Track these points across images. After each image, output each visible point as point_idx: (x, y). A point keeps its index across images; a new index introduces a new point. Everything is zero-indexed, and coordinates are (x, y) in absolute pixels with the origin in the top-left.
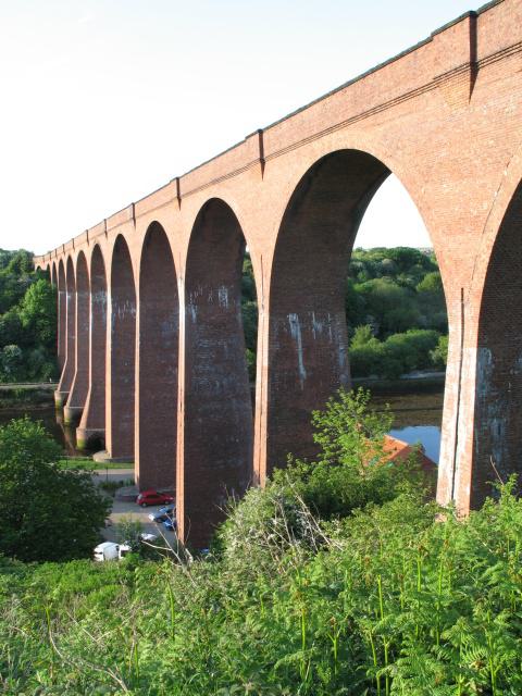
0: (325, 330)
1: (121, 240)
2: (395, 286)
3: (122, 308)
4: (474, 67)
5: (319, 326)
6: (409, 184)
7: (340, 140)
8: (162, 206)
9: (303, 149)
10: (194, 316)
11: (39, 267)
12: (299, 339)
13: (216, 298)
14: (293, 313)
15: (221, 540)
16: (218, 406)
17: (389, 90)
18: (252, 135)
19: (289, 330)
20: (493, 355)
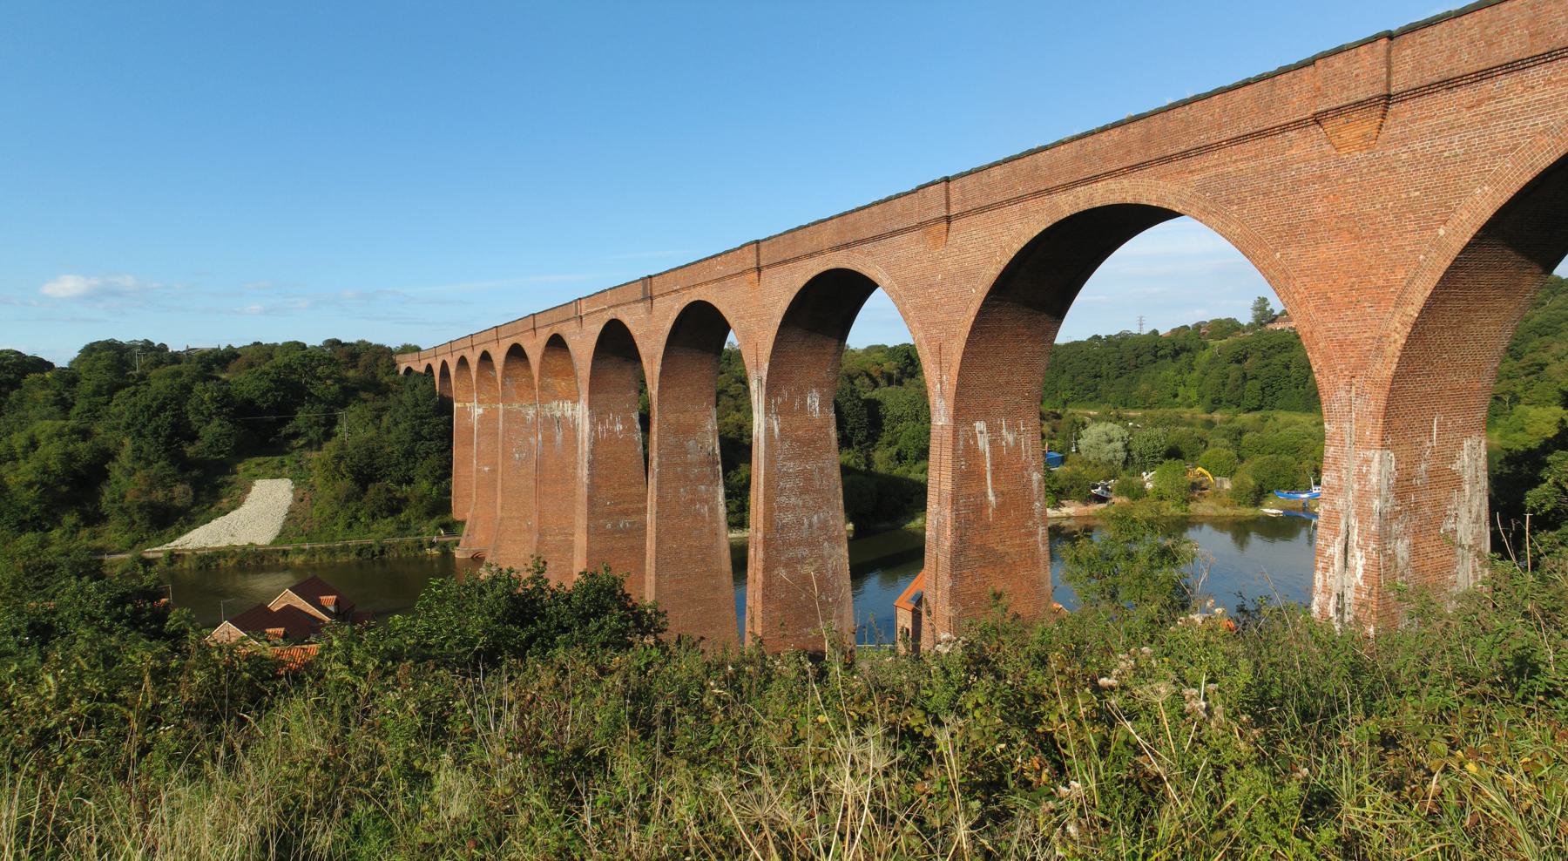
0: (1017, 444)
3: (603, 424)
5: (1010, 438)
6: (890, 292)
9: (1046, 201)
10: (777, 430)
13: (803, 406)
15: (62, 463)
19: (976, 442)
20: (1398, 460)
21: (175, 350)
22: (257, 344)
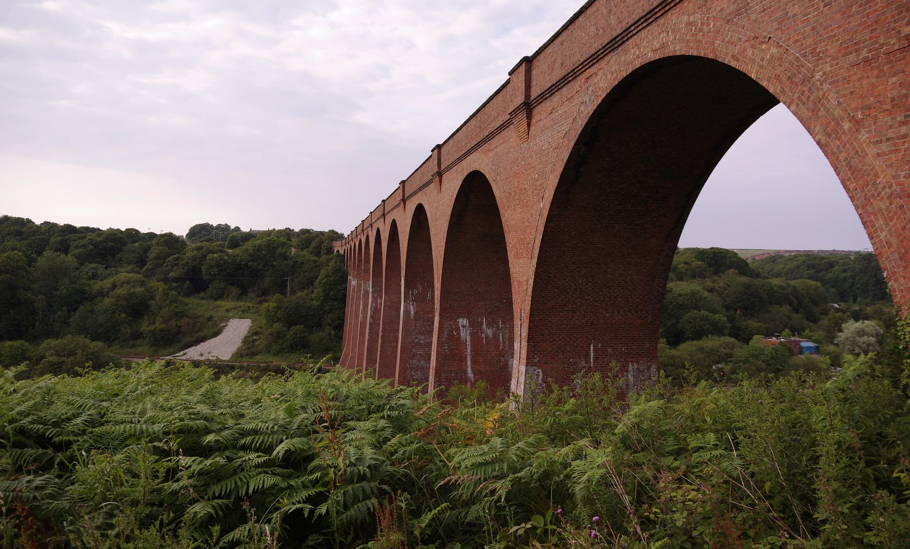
0: (496, 337)
2: (111, 299)
4: (440, 174)
5: (490, 332)
10: (412, 312)
11: (338, 251)
14: (463, 317)
19: (459, 334)
21: (187, 232)
22: (171, 234)
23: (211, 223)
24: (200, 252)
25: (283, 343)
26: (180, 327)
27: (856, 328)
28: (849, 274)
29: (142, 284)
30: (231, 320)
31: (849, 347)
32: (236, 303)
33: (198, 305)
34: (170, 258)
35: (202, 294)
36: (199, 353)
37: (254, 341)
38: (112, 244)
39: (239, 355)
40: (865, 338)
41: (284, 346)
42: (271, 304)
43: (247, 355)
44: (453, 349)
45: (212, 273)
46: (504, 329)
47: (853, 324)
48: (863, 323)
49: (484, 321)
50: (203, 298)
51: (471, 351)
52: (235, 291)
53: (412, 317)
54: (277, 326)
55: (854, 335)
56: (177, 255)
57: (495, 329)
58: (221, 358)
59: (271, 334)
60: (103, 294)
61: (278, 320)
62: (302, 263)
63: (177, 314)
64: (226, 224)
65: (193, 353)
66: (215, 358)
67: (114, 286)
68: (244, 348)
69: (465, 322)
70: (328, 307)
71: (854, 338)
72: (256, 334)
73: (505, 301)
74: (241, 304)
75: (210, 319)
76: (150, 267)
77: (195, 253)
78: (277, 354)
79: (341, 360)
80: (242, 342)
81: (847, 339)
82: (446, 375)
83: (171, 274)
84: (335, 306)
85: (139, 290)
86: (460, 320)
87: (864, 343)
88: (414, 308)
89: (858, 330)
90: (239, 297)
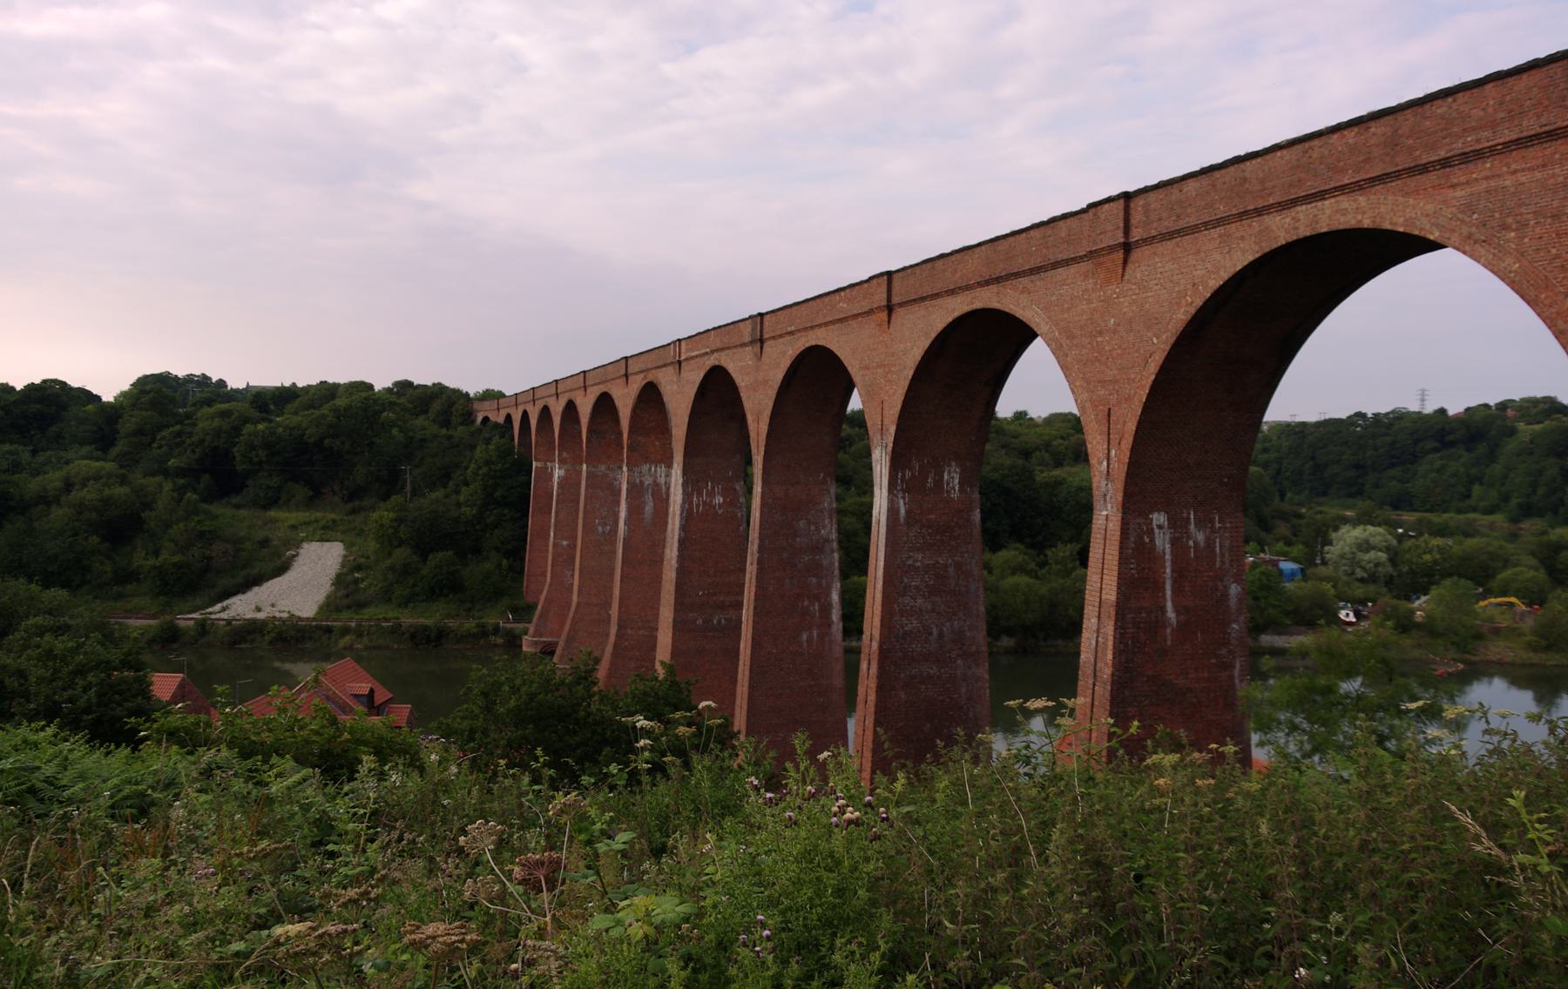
0: (1210, 545)
1: (525, 413)
3: (700, 494)
5: (1200, 537)
7: (1344, 212)
8: (841, 320)
10: (903, 511)
12: (1168, 557)
13: (939, 482)
14: (1159, 511)
16: (934, 671)
17: (1493, 125)
18: (1109, 200)
19: (1152, 540)
23: (174, 372)
24: (227, 420)
25: (414, 585)
26: (210, 558)
27: (1357, 538)
28: (1273, 455)
29: (123, 480)
30: (305, 545)
31: (1347, 568)
32: (307, 514)
33: (234, 517)
34: (165, 433)
35: (236, 500)
36: (253, 607)
37: (356, 581)
38: (39, 406)
39: (330, 606)
40: (1372, 555)
41: (417, 589)
42: (383, 514)
43: (349, 607)
44: (1144, 568)
45: (256, 459)
46: (1222, 531)
47: (1348, 531)
48: (1365, 530)
49: (1192, 517)
50: (238, 507)
51: (1173, 571)
52: (301, 492)
53: (902, 520)
54: (402, 554)
55: (1355, 550)
56: (178, 427)
57: (1208, 530)
58: (297, 613)
59: (392, 568)
60: (46, 500)
61: (401, 543)
62: (424, 440)
63: (202, 535)
64: (203, 374)
65: (242, 607)
66: (285, 615)
67: (68, 486)
68: (339, 594)
69: (1162, 520)
70: (492, 518)
71: (1353, 553)
72: (359, 568)
73: (1226, 480)
74: (319, 515)
75: (265, 543)
76: (126, 449)
77: (217, 422)
78: (405, 603)
79: (538, 612)
80: (332, 584)
81: (1342, 556)
82: (1132, 615)
83: (172, 462)
84: (505, 515)
85: (120, 491)
86: (1155, 516)
87: (1369, 562)
88: (905, 504)
89: (1359, 541)
90: (310, 503)
